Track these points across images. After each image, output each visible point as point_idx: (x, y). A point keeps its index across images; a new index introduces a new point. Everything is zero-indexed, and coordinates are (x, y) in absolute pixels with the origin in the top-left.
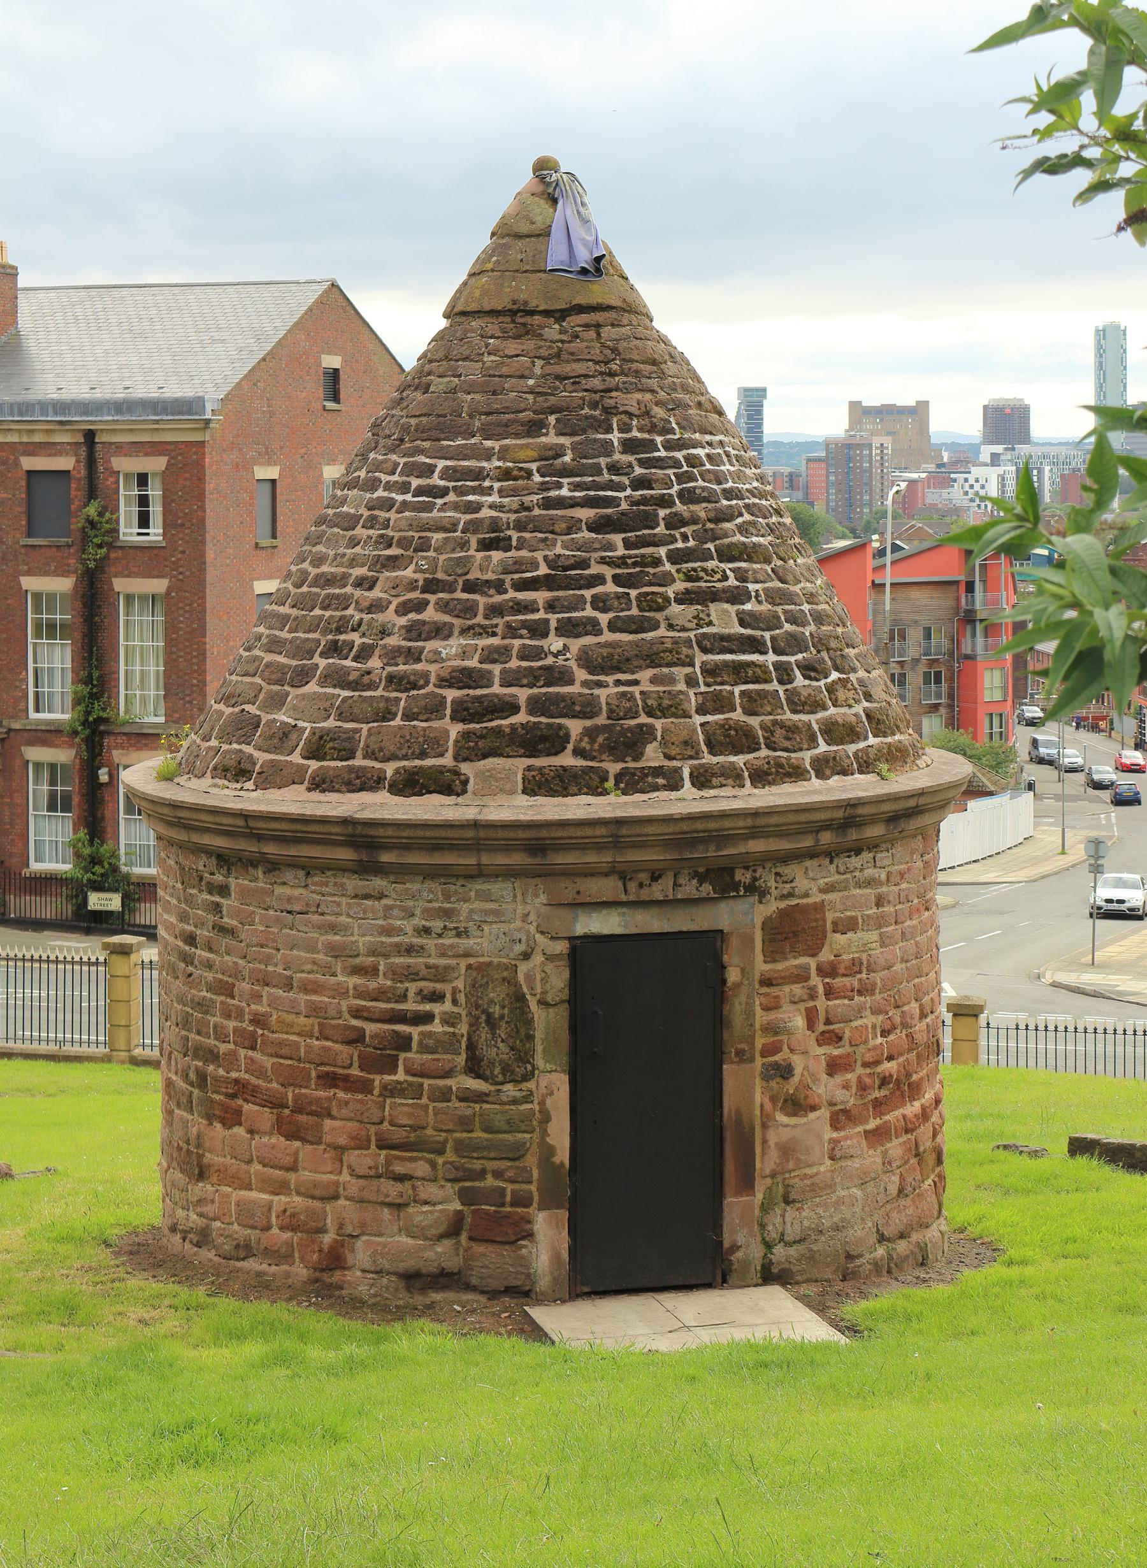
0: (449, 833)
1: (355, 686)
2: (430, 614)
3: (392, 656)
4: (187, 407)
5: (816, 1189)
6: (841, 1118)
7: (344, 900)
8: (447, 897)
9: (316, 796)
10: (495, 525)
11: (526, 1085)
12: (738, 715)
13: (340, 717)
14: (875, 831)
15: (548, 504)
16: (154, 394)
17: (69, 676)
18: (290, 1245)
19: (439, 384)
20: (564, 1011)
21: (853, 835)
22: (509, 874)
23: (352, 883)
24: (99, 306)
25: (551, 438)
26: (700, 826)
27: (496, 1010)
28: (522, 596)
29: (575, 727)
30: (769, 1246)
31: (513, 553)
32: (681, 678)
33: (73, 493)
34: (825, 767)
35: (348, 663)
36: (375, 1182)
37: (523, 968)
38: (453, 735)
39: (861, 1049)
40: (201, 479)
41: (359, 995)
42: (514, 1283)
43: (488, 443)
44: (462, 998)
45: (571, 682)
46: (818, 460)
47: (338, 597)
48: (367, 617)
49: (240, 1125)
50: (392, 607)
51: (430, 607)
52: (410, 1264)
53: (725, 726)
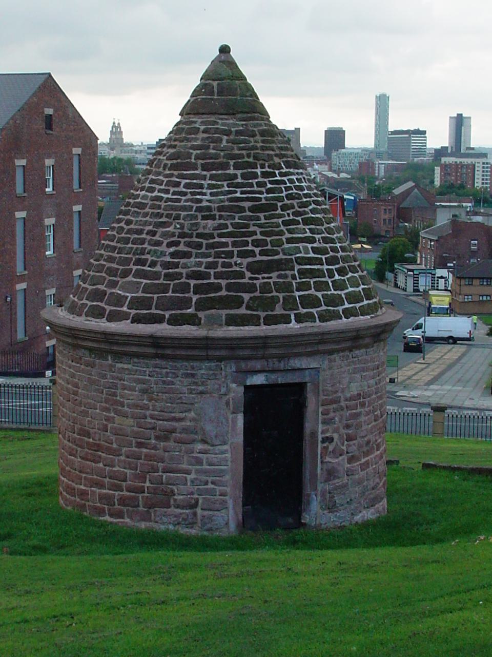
2: (182, 248)
9: (135, 325)
10: (209, 209)
12: (312, 292)
29: (246, 297)
34: (348, 313)
38: (194, 300)
50: (165, 244)
51: (182, 244)
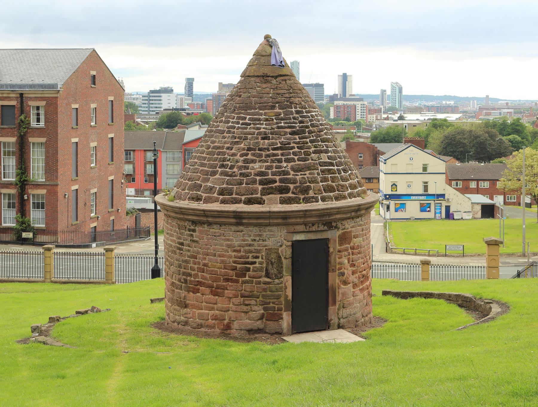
0: (263, 214)
1: (231, 176)
2: (250, 157)
3: (240, 168)
4: (53, 86)
5: (350, 304)
6: (355, 286)
7: (231, 233)
8: (260, 231)
9: (223, 205)
10: (265, 133)
11: (281, 280)
12: (330, 183)
13: (227, 184)
14: (363, 212)
15: (279, 128)
16: (41, 82)
17: (15, 167)
18: (214, 324)
19: (244, 95)
20: (290, 260)
21: (359, 213)
22: (277, 225)
23: (234, 228)
24: (21, 55)
25: (277, 110)
26: (325, 211)
27: (273, 260)
28: (274, 152)
29: (292, 186)
30: (339, 319)
31: (271, 141)
32: (316, 173)
33: (16, 112)
34: (351, 196)
35: (227, 170)
36: (240, 306)
37: (280, 249)
38: (260, 189)
39: (359, 268)
40: (57, 108)
41: (235, 257)
42: (278, 331)
43: (261, 111)
44: (264, 257)
45: (290, 175)
46: (210, 100)
47: (222, 152)
48: (232, 158)
49: (199, 292)
50: (239, 155)
51: (250, 155)
52: (249, 327)
53: (327, 185)
